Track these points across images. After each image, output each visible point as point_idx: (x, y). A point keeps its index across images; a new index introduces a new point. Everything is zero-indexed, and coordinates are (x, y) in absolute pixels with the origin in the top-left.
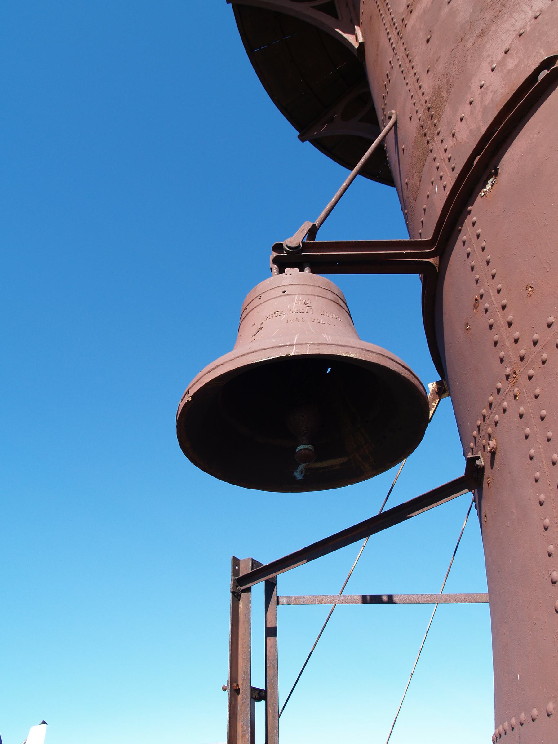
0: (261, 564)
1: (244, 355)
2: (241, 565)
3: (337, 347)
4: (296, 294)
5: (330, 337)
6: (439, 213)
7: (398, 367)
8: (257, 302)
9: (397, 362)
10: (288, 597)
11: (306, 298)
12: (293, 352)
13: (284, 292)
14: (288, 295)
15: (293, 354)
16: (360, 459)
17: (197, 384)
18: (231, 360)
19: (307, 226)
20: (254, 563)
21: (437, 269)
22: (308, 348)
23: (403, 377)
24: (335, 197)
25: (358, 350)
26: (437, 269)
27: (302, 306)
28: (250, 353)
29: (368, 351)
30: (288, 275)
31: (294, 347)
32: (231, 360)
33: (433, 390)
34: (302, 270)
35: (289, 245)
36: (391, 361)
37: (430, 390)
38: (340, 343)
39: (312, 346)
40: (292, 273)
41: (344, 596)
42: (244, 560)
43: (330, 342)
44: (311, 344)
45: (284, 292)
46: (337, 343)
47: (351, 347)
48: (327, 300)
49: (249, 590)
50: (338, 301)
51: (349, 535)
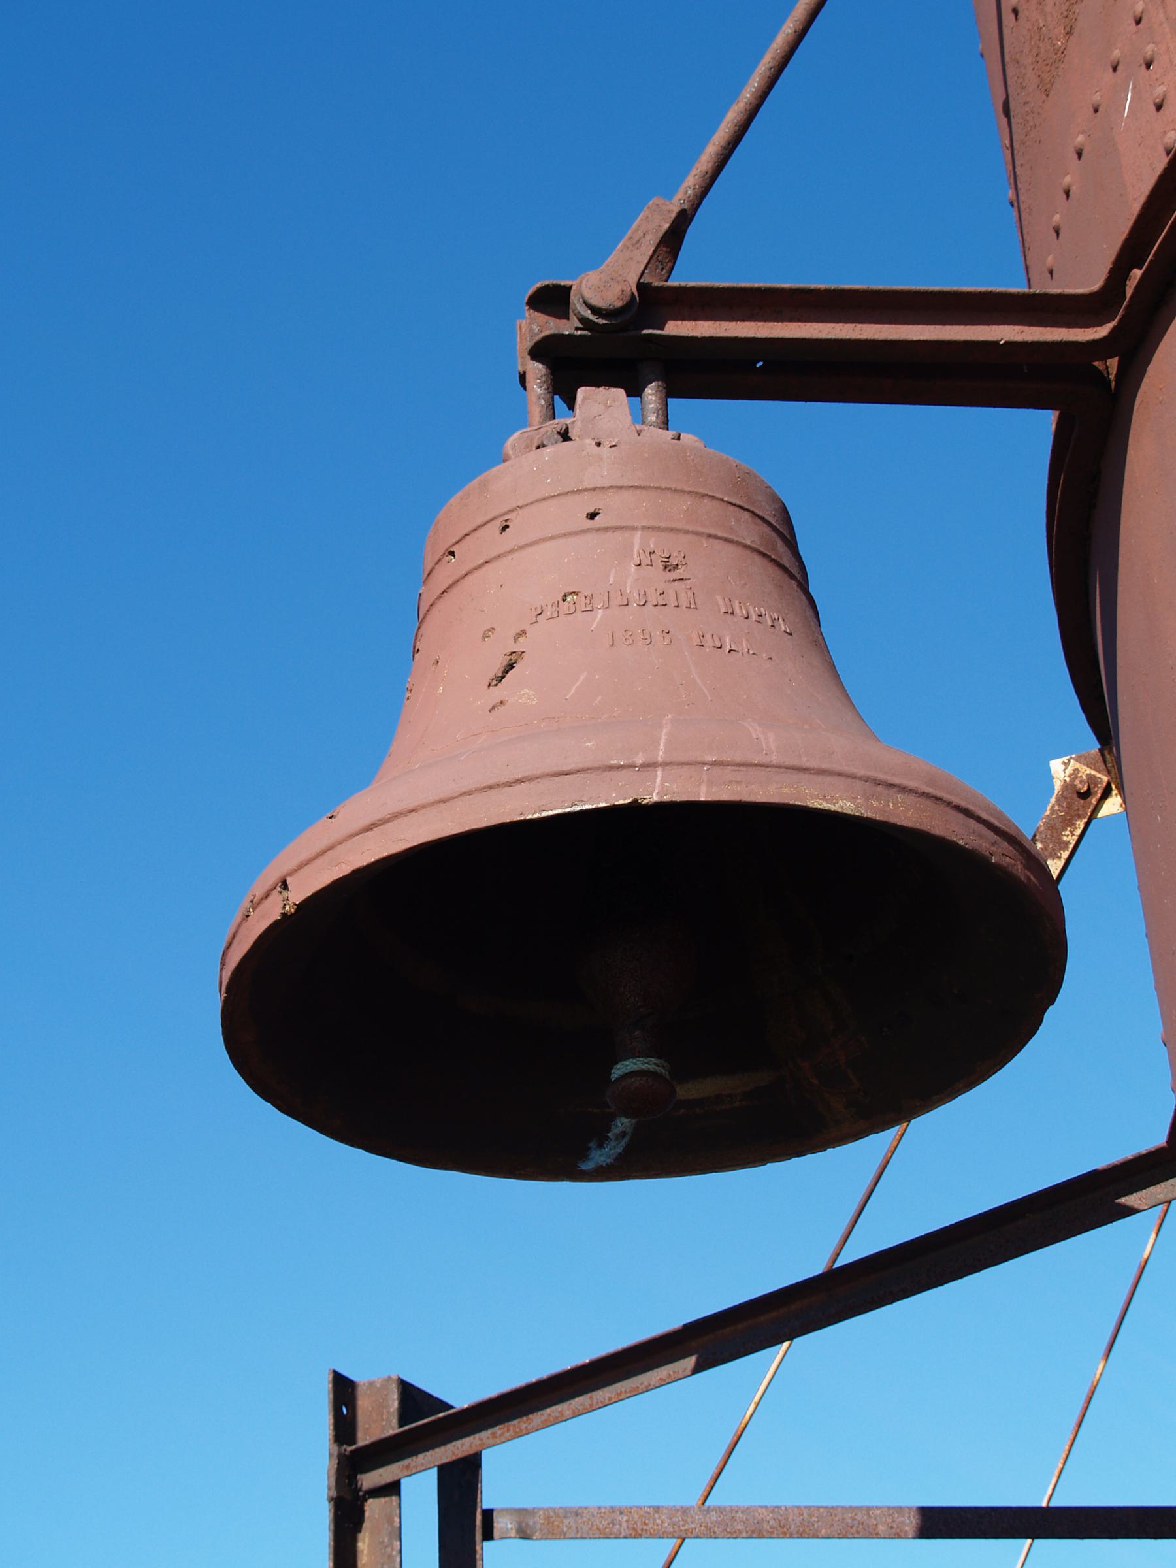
0: (449, 1407)
1: (490, 787)
2: (364, 1404)
3: (795, 776)
4: (634, 528)
5: (771, 736)
6: (1136, 208)
7: (981, 836)
8: (490, 541)
9: (979, 819)
10: (521, 1512)
11: (675, 546)
12: (657, 789)
13: (592, 516)
14: (606, 529)
15: (655, 799)
16: (816, 1082)
17: (318, 862)
18: (444, 801)
19: (653, 221)
20: (413, 1400)
21: (1113, 384)
22: (705, 778)
23: (997, 866)
24: (755, 83)
25: (859, 783)
26: (1113, 384)
27: (657, 573)
28: (509, 784)
29: (892, 785)
30: (605, 450)
31: (659, 773)
32: (444, 801)
33: (1066, 786)
34: (634, 391)
35: (596, 301)
36: (961, 816)
37: (1058, 785)
38: (805, 762)
39: (717, 770)
40: (602, 407)
41: (720, 1510)
42: (371, 1384)
43: (774, 758)
44: (715, 764)
45: (592, 516)
46: (796, 762)
47: (840, 774)
48: (739, 551)
49: (392, 1489)
50: (774, 549)
51: (762, 1319)
